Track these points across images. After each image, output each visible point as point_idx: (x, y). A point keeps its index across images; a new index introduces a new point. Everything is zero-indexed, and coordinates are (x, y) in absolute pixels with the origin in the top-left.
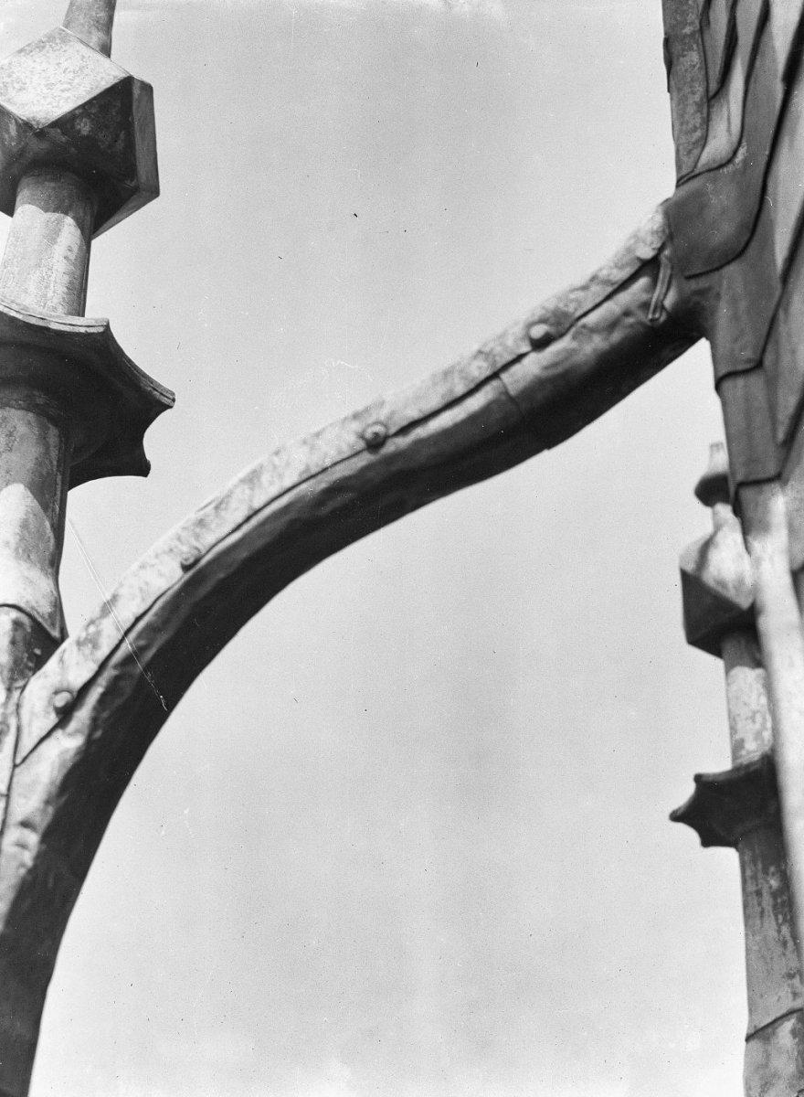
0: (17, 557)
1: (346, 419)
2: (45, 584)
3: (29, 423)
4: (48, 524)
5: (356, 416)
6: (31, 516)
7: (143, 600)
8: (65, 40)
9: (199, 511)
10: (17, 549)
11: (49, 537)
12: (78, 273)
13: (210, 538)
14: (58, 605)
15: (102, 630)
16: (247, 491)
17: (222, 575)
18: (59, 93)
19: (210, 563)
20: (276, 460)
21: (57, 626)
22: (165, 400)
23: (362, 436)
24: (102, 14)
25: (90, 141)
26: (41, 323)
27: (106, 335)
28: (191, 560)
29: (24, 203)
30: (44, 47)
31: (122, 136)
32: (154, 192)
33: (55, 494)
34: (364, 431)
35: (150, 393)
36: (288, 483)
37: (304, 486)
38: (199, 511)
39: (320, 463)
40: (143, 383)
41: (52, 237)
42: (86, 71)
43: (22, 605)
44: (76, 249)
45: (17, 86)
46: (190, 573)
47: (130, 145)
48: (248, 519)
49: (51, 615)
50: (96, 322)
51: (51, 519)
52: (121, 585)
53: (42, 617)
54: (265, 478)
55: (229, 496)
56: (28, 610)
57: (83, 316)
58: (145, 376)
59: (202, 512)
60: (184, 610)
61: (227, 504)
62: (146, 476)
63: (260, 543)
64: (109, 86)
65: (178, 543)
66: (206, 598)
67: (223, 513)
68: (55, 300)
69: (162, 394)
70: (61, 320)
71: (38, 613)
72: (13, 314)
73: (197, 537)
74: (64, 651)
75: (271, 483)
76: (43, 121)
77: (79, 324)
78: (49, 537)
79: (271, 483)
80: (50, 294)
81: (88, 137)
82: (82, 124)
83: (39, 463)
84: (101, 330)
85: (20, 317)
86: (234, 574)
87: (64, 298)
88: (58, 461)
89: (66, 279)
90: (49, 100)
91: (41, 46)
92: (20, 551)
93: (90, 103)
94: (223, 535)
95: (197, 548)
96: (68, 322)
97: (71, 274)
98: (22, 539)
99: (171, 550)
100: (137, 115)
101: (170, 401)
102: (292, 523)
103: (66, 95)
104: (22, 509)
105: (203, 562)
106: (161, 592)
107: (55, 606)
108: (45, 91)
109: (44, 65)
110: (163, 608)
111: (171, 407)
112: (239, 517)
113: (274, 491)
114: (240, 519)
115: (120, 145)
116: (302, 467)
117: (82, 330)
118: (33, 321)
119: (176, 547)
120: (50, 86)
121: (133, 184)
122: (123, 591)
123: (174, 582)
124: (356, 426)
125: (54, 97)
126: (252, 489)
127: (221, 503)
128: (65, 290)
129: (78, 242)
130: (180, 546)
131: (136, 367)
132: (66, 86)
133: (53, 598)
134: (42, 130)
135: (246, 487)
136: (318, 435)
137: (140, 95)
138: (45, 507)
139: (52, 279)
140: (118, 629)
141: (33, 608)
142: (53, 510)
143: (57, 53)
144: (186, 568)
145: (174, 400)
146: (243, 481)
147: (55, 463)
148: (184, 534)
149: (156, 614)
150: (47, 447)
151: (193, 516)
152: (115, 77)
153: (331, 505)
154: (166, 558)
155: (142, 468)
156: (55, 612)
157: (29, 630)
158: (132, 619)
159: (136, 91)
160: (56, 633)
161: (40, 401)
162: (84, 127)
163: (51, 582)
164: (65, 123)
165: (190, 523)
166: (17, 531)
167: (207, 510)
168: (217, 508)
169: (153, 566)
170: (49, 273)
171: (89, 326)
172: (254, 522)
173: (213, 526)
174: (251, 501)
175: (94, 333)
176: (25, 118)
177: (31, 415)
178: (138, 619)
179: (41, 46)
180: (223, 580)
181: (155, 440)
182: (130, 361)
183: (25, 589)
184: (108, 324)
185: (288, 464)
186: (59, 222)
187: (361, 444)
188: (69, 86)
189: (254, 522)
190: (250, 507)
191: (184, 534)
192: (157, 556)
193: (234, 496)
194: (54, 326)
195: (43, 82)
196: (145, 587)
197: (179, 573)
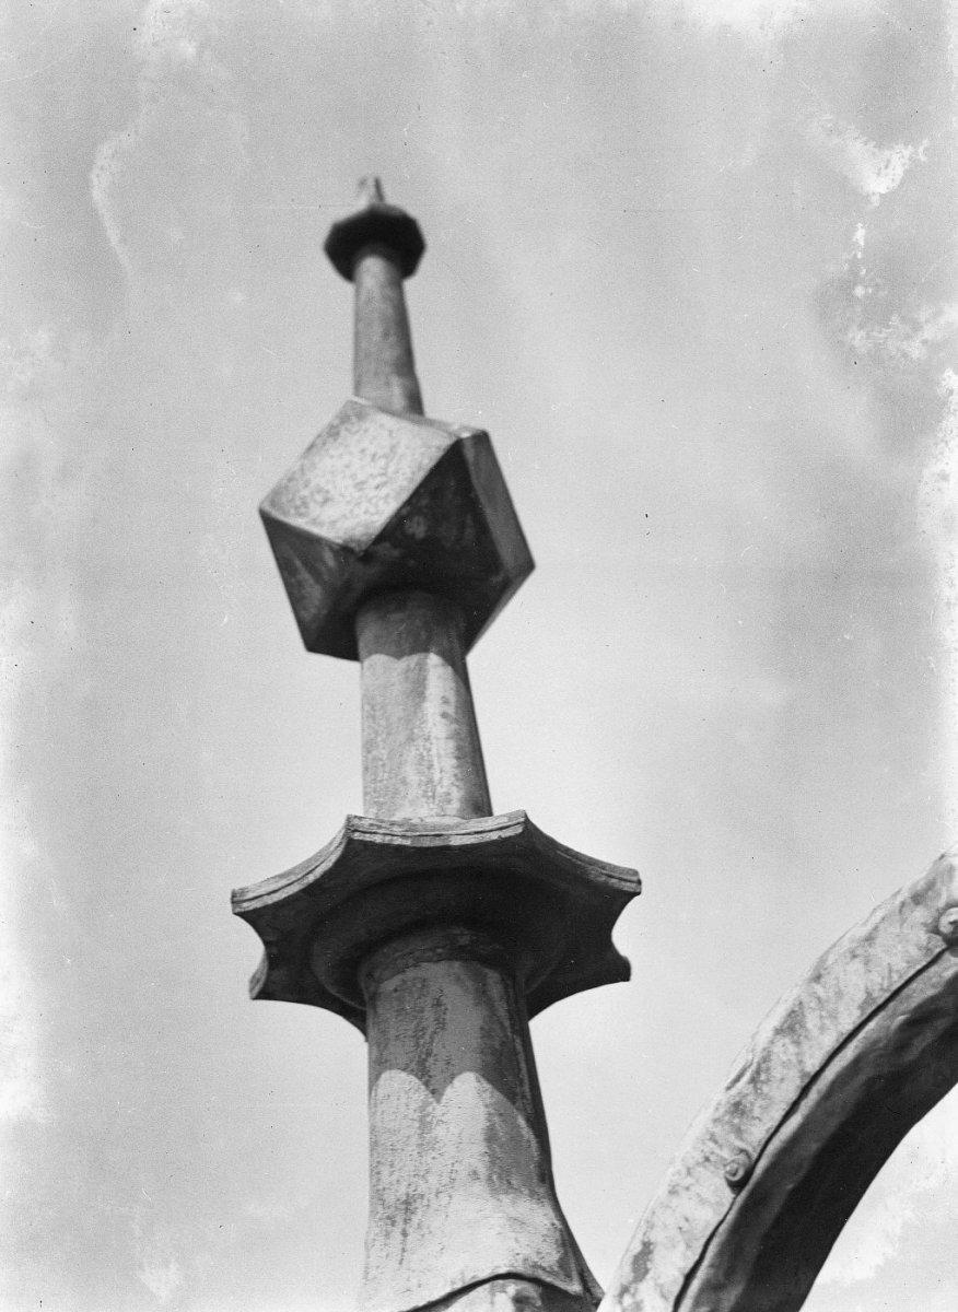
0: (494, 1192)
1: (903, 904)
2: (542, 1217)
3: (458, 979)
4: (521, 1121)
5: (918, 899)
6: (496, 1119)
7: (688, 1246)
8: (361, 416)
9: (729, 1088)
10: (490, 1178)
11: (528, 1141)
12: (465, 730)
13: (758, 1133)
14: (568, 1242)
15: (642, 1301)
16: (792, 1049)
17: (790, 1186)
18: (372, 493)
19: (768, 1171)
20: (819, 989)
21: (575, 1275)
22: (628, 887)
23: (935, 930)
24: (389, 292)
25: (431, 542)
26: (438, 843)
27: (529, 829)
28: (741, 1173)
29: (370, 654)
30: (338, 434)
31: (469, 521)
32: (527, 566)
33: (520, 1070)
34: (937, 920)
35: (606, 883)
36: (847, 1025)
37: (872, 1025)
38: (729, 1088)
39: (885, 985)
40: (593, 874)
41: (418, 691)
42: (400, 451)
43: (520, 1269)
44: (452, 698)
45: (319, 498)
46: (744, 1194)
47: (483, 529)
48: (805, 1091)
49: (562, 1263)
50: (506, 819)
51: (523, 1110)
52: (650, 1225)
53: (551, 1273)
54: (812, 1021)
55: (766, 1059)
56: (529, 1272)
57: (490, 814)
58: (593, 862)
59: (734, 1091)
60: (752, 1249)
61: (768, 1069)
62: (628, 980)
63: (833, 1124)
64: (433, 463)
65: (711, 1145)
66: (778, 1221)
67: (765, 1089)
68: (446, 782)
69: (621, 879)
70: (464, 832)
71: (544, 1269)
72: (398, 841)
73: (739, 1132)
74: (865, 924)
75: (822, 1029)
76: (364, 538)
77: (487, 829)
78: (528, 1141)
79: (822, 1029)
80: (437, 776)
81: (424, 541)
82: (415, 525)
83: (486, 1033)
84: (519, 830)
85: (408, 843)
86: (807, 1179)
87: (455, 775)
88: (510, 1019)
89: (451, 744)
90: (364, 506)
91: (333, 432)
92: (495, 1177)
93: (416, 494)
94: (776, 1124)
95: (742, 1151)
96: (474, 830)
97: (455, 735)
98: (494, 1160)
99: (707, 1159)
100: (478, 482)
101: (634, 885)
102: (871, 1082)
103: (384, 491)
104: (481, 1112)
105: (759, 1170)
106: (708, 1233)
107: (563, 1245)
108: (357, 494)
109: (346, 459)
110: (720, 1253)
111: (639, 894)
112: (790, 1091)
113: (829, 1041)
114: (793, 1096)
115: (470, 532)
116: (861, 996)
117: (494, 836)
118: (427, 843)
119: (712, 1153)
120: (360, 486)
121: (499, 578)
122: (657, 1236)
123: (725, 1209)
124: (920, 915)
125: (370, 501)
126: (797, 1043)
127: (758, 1072)
128: (454, 762)
129: (453, 685)
130: (717, 1151)
131: (577, 856)
132: (379, 480)
133: (558, 1234)
134: (366, 551)
135: (787, 1040)
136: (870, 939)
137: (477, 455)
138: (511, 1095)
139: (434, 752)
140: (663, 1296)
141: (535, 1266)
142: (524, 1097)
143: (356, 437)
144: (737, 1186)
145: (639, 882)
146: (779, 1031)
147: (507, 1023)
148: (718, 1130)
149: (712, 1266)
150: (490, 1004)
151: (719, 1097)
152: (438, 448)
153: (920, 1044)
154: (702, 1172)
155: (619, 970)
156: (566, 1253)
157: (539, 1303)
158: (681, 1281)
159: (469, 454)
160: (575, 1287)
161: (464, 940)
162: (418, 529)
163: (549, 1210)
164: (394, 531)
165: (722, 1110)
166: (482, 1147)
167: (740, 1085)
168: (753, 1080)
169: (687, 1189)
170: (428, 745)
171: (501, 829)
172: (813, 1096)
173: (757, 1112)
174: (800, 1062)
175: (510, 837)
176: (340, 541)
177: (457, 964)
178: (689, 1277)
179: (333, 432)
180: (794, 1191)
181: (626, 935)
182: (567, 850)
183: (517, 1240)
184: (526, 816)
185: (839, 994)
186: (421, 667)
187: (938, 945)
188: (384, 479)
189: (813, 1096)
190: (803, 1074)
191: (718, 1130)
192: (689, 1172)
193: (774, 1063)
194: (456, 841)
195: (350, 482)
196: (686, 1226)
197: (728, 1194)
